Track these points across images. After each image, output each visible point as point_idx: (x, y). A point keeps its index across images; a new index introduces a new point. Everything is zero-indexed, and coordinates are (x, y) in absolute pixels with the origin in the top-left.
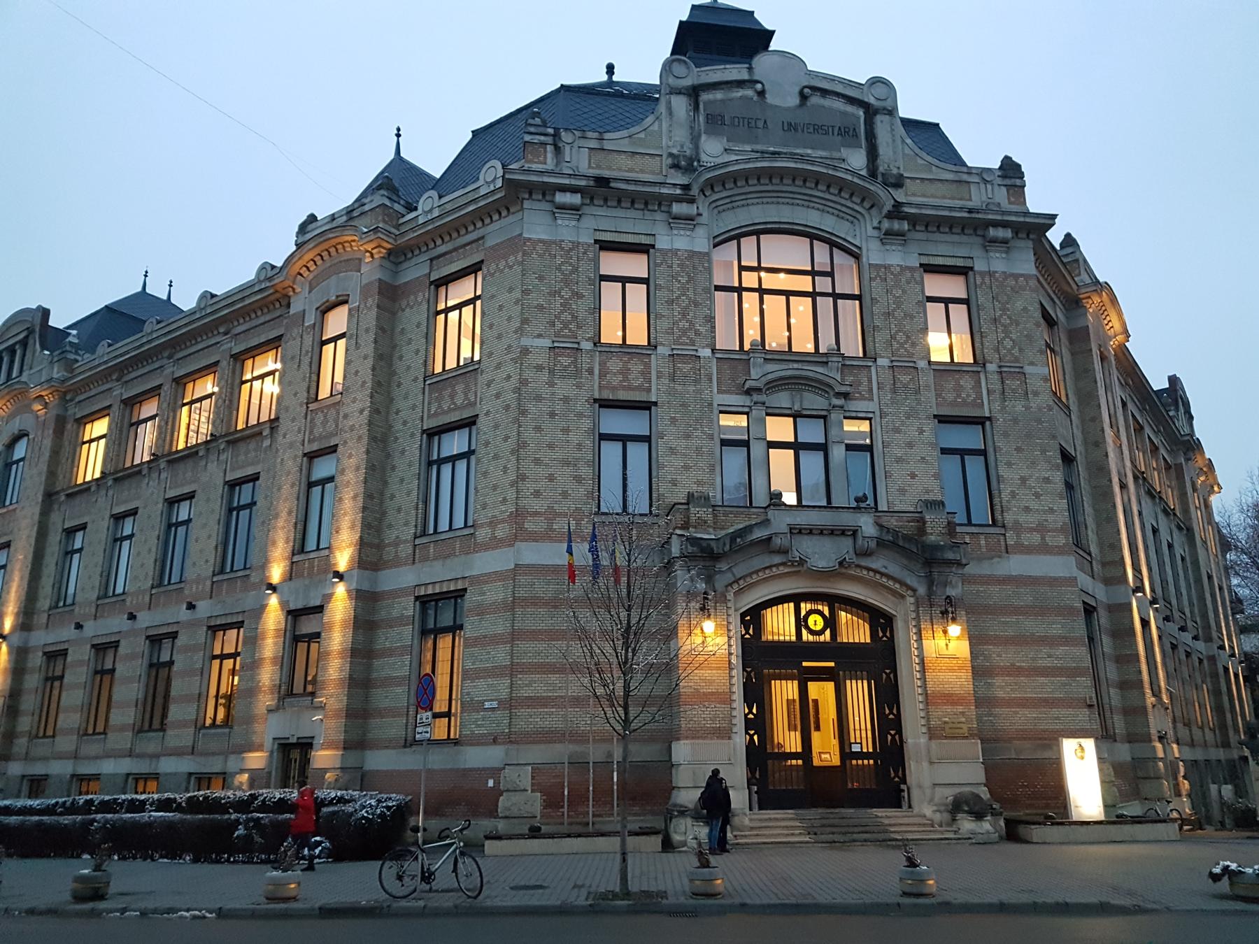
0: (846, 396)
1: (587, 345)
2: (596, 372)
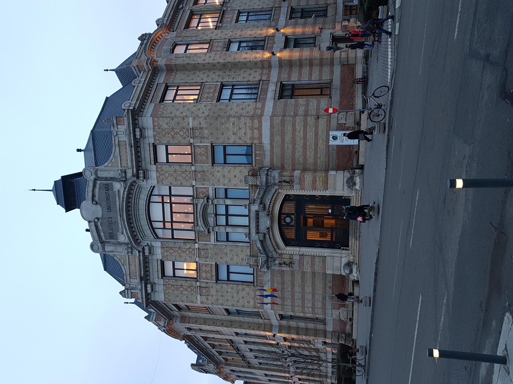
0: (208, 198)
1: (193, 168)
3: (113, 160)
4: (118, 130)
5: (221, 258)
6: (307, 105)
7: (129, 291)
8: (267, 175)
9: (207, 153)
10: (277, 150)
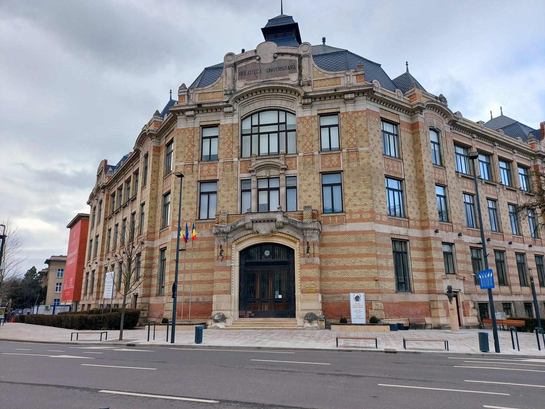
0: (286, 169)
1: (316, 153)
2: (199, 171)
3: (320, 73)
4: (351, 77)
5: (224, 185)
6: (388, 268)
7: (186, 93)
8: (314, 229)
9: (333, 166)
10: (339, 239)
